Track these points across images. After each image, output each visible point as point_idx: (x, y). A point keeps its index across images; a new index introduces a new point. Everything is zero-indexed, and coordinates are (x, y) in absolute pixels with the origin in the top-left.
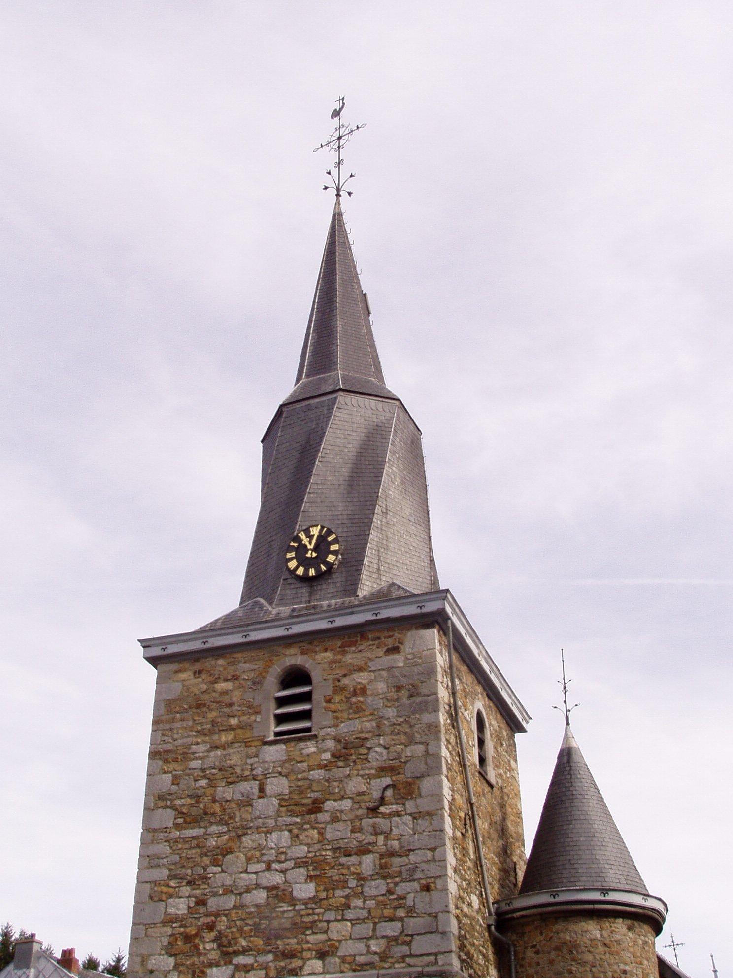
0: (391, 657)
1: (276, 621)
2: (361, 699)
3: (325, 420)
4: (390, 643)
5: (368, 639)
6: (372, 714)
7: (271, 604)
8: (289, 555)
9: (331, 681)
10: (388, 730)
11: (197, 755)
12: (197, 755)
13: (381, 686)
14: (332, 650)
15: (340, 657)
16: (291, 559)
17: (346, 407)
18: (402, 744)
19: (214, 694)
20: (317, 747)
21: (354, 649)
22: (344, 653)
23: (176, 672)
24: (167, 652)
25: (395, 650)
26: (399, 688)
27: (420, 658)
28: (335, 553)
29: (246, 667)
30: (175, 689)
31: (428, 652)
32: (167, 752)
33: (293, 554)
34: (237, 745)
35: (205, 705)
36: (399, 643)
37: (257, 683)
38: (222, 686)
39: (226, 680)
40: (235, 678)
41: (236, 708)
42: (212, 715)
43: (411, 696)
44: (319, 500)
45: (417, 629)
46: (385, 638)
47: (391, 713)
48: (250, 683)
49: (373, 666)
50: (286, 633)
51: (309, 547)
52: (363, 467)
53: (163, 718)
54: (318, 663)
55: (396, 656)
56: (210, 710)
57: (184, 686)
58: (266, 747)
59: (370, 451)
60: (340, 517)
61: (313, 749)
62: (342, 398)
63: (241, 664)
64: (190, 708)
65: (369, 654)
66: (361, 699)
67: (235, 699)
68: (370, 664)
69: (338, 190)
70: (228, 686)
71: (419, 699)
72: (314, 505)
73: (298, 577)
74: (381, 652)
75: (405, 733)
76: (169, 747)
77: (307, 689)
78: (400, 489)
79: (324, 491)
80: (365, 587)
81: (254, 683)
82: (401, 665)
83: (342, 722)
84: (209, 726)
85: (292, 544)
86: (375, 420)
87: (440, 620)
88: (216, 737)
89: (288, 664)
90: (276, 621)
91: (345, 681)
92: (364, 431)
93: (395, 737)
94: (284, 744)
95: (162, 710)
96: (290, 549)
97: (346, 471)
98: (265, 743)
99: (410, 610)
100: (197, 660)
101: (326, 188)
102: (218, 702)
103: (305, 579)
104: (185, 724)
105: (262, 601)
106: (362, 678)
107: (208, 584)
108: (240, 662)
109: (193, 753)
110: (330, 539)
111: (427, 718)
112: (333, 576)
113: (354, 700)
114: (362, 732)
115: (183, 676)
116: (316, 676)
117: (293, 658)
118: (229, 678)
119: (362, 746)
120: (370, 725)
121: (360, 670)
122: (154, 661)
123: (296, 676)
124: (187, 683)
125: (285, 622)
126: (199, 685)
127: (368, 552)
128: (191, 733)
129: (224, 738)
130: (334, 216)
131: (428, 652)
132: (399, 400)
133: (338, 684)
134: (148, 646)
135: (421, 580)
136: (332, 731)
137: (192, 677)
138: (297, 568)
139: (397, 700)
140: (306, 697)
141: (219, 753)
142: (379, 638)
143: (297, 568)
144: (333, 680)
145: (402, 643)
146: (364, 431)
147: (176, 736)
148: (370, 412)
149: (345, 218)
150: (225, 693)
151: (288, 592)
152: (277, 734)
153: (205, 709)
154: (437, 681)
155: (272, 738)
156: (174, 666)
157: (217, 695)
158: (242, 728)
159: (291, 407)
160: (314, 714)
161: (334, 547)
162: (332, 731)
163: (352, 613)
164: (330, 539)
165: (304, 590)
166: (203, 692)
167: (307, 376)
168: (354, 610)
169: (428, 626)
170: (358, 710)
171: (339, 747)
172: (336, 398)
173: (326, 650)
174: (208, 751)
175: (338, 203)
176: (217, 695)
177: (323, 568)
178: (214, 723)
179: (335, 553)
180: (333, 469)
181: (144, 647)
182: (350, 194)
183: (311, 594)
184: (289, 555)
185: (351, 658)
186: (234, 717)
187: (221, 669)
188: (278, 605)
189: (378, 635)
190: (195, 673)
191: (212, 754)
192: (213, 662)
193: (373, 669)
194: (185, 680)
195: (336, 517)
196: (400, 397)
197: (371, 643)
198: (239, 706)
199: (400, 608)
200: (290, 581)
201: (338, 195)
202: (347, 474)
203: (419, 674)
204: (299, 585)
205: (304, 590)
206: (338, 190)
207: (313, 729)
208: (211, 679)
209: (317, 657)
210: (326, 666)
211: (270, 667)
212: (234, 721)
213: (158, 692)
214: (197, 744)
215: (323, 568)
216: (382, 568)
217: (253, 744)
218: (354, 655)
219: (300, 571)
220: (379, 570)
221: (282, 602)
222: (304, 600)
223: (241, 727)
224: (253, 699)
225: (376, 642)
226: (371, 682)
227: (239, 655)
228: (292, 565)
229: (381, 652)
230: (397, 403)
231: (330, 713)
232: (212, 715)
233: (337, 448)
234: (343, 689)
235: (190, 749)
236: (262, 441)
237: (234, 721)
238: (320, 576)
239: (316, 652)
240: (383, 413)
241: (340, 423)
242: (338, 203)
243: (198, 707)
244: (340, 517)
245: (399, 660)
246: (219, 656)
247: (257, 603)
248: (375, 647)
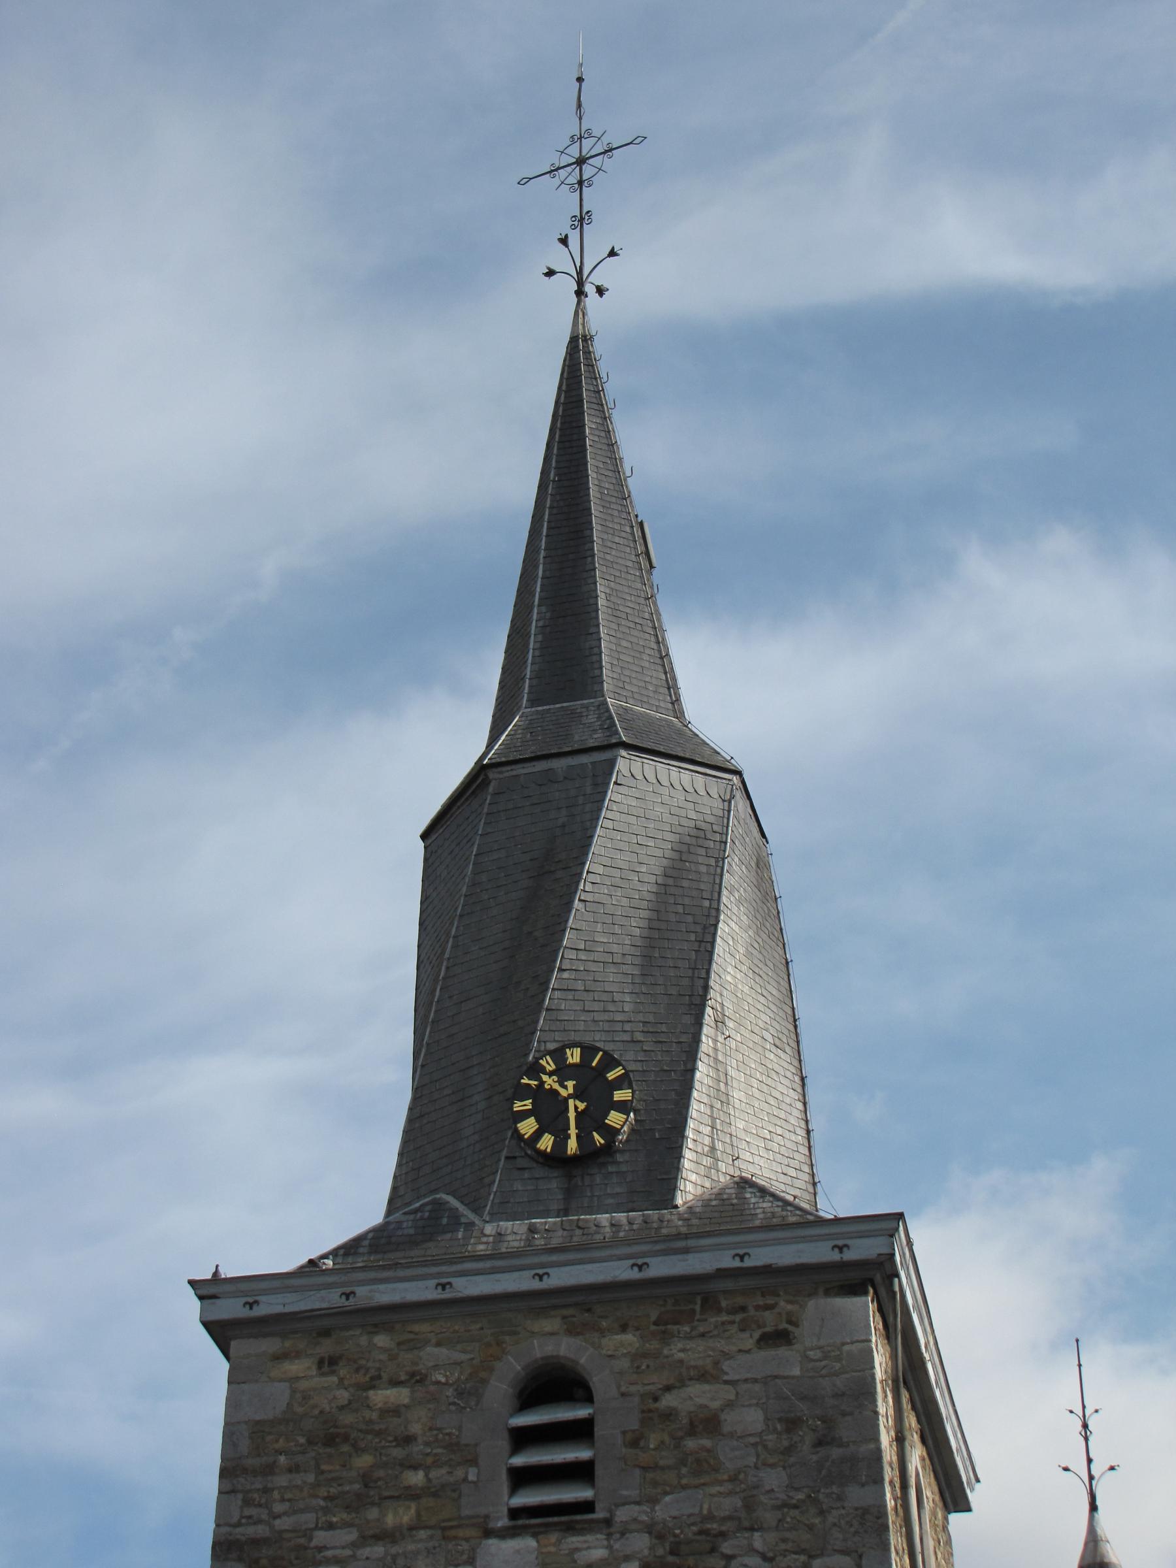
0: (771, 1353)
1: (500, 1259)
2: (707, 1443)
3: (588, 807)
4: (770, 1322)
5: (719, 1310)
6: (733, 1479)
7: (478, 1210)
8: (518, 1106)
9: (637, 1400)
10: (770, 1518)
11: (329, 1553)
12: (329, 1553)
13: (751, 1419)
14: (637, 1329)
15: (653, 1345)
16: (524, 1115)
17: (632, 783)
18: (802, 1551)
19: (367, 1414)
20: (609, 1547)
21: (687, 1329)
22: (665, 1337)
23: (278, 1358)
24: (260, 1311)
25: (779, 1338)
26: (792, 1424)
27: (838, 1359)
28: (623, 1107)
29: (440, 1358)
30: (276, 1398)
31: (854, 1348)
32: (256, 1542)
33: (528, 1104)
34: (423, 1534)
35: (346, 1438)
36: (790, 1322)
37: (469, 1391)
38: (383, 1396)
39: (395, 1383)
40: (417, 1379)
41: (417, 1448)
42: (364, 1461)
43: (820, 1443)
44: (580, 986)
45: (828, 1293)
46: (757, 1308)
47: (774, 1479)
48: (450, 1392)
49: (732, 1369)
50: (536, 1285)
51: (564, 1093)
52: (673, 918)
53: (250, 1462)
54: (606, 1358)
55: (783, 1352)
56: (358, 1450)
57: (294, 1391)
58: (493, 1542)
59: (685, 883)
60: (627, 1027)
61: (598, 1554)
62: (626, 763)
63: (429, 1349)
64: (310, 1442)
65: (721, 1344)
66: (707, 1443)
67: (416, 1428)
68: (726, 1366)
69: (580, 283)
70: (400, 1395)
71: (836, 1452)
72: (570, 996)
73: (543, 1154)
74: (748, 1340)
75: (811, 1528)
76: (261, 1531)
77: (582, 1412)
78: (744, 968)
79: (592, 967)
80: (690, 1187)
81: (460, 1394)
82: (796, 1372)
83: (666, 1493)
84: (357, 1486)
85: (525, 1081)
86: (692, 815)
87: (878, 1278)
88: (373, 1513)
89: (538, 1354)
90: (500, 1259)
91: (668, 1401)
92: (670, 837)
93: (788, 1535)
94: (535, 1535)
95: (244, 1446)
96: (522, 1092)
97: (636, 925)
98: (488, 1533)
99: (820, 1253)
100: (326, 1333)
101: (550, 273)
102: (378, 1433)
103: (557, 1160)
104: (298, 1479)
105: (454, 1202)
106: (698, 1396)
107: (302, 1153)
108: (427, 1342)
109: (321, 1549)
110: (611, 1076)
111: (856, 1496)
112: (619, 1158)
113: (691, 1444)
114: (710, 1517)
115: (294, 1367)
116: (600, 1383)
117: (550, 1342)
118: (403, 1378)
119: (713, 1550)
120: (729, 1504)
121: (703, 1376)
122: (221, 1332)
123: (553, 1383)
124: (303, 1385)
125: (536, 1260)
126: (331, 1393)
127: (694, 1106)
128: (314, 1502)
129: (399, 1516)
130: (574, 340)
131: (854, 1348)
132: (738, 773)
133: (653, 1406)
134: (214, 1297)
135: (793, 1173)
136: (640, 1512)
137: (314, 1367)
138: (537, 1135)
139: (789, 1450)
140: (581, 1431)
141: (378, 1550)
142: (743, 1309)
143: (537, 1135)
144: (643, 1396)
145: (796, 1325)
146: (670, 837)
147: (278, 1508)
148: (681, 796)
149: (599, 348)
150: (395, 1411)
151: (518, 1186)
152: (514, 1513)
153: (346, 1448)
154: (876, 1413)
155: (503, 1522)
156: (270, 1345)
157: (375, 1416)
158: (435, 1495)
159: (508, 772)
160: (599, 1471)
161: (620, 1095)
162: (640, 1512)
163: (686, 1251)
164: (611, 1076)
165: (554, 1184)
166: (341, 1408)
167: (533, 702)
168: (691, 1243)
169: (856, 1289)
170: (703, 1467)
171: (660, 1552)
172: (612, 763)
173: (624, 1328)
174: (353, 1545)
175: (580, 311)
176: (375, 1416)
177: (598, 1139)
178: (367, 1479)
179: (623, 1107)
180: (609, 920)
181: (201, 1298)
182: (600, 291)
183: (569, 1193)
184: (518, 1106)
185: (686, 1350)
186: (415, 1468)
187: (383, 1357)
188: (495, 1216)
189: (740, 1300)
190: (320, 1363)
191: (366, 1552)
192: (363, 1340)
193: (731, 1376)
194: (298, 1378)
195: (618, 1027)
196: (740, 763)
197: (725, 1318)
198: (427, 1444)
199: (794, 1247)
200: (521, 1163)
201: (580, 293)
202: (637, 932)
203: (836, 1396)
204: (540, 1172)
205: (553, 1184)
206: (580, 283)
207: (598, 1506)
208: (362, 1378)
209: (604, 1341)
210: (625, 1364)
211: (499, 1359)
212: (416, 1478)
213: (233, 1404)
214: (331, 1526)
215: (598, 1139)
216: (719, 1146)
217: (461, 1533)
218: (690, 1345)
219: (546, 1143)
220: (713, 1148)
221: (504, 1211)
222: (555, 1206)
223: (431, 1491)
224: (460, 1429)
225: (738, 1318)
226: (730, 1405)
227: (424, 1328)
228: (528, 1127)
229: (748, 1340)
230: (736, 779)
231: (637, 1471)
232: (364, 1461)
233: (617, 873)
234: (669, 1415)
235: (311, 1539)
236: (424, 836)
237: (416, 1478)
238: (590, 1156)
239: (602, 1332)
240: (706, 799)
241: (624, 817)
242: (580, 311)
243: (330, 1440)
244: (627, 1027)
245: (788, 1363)
246: (377, 1328)
247: (439, 1206)
248: (734, 1329)
